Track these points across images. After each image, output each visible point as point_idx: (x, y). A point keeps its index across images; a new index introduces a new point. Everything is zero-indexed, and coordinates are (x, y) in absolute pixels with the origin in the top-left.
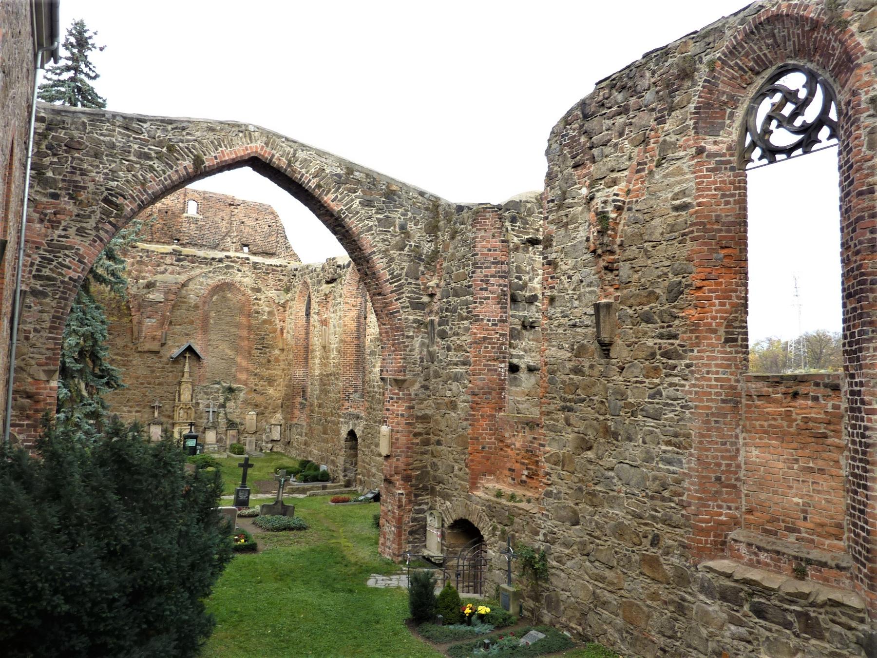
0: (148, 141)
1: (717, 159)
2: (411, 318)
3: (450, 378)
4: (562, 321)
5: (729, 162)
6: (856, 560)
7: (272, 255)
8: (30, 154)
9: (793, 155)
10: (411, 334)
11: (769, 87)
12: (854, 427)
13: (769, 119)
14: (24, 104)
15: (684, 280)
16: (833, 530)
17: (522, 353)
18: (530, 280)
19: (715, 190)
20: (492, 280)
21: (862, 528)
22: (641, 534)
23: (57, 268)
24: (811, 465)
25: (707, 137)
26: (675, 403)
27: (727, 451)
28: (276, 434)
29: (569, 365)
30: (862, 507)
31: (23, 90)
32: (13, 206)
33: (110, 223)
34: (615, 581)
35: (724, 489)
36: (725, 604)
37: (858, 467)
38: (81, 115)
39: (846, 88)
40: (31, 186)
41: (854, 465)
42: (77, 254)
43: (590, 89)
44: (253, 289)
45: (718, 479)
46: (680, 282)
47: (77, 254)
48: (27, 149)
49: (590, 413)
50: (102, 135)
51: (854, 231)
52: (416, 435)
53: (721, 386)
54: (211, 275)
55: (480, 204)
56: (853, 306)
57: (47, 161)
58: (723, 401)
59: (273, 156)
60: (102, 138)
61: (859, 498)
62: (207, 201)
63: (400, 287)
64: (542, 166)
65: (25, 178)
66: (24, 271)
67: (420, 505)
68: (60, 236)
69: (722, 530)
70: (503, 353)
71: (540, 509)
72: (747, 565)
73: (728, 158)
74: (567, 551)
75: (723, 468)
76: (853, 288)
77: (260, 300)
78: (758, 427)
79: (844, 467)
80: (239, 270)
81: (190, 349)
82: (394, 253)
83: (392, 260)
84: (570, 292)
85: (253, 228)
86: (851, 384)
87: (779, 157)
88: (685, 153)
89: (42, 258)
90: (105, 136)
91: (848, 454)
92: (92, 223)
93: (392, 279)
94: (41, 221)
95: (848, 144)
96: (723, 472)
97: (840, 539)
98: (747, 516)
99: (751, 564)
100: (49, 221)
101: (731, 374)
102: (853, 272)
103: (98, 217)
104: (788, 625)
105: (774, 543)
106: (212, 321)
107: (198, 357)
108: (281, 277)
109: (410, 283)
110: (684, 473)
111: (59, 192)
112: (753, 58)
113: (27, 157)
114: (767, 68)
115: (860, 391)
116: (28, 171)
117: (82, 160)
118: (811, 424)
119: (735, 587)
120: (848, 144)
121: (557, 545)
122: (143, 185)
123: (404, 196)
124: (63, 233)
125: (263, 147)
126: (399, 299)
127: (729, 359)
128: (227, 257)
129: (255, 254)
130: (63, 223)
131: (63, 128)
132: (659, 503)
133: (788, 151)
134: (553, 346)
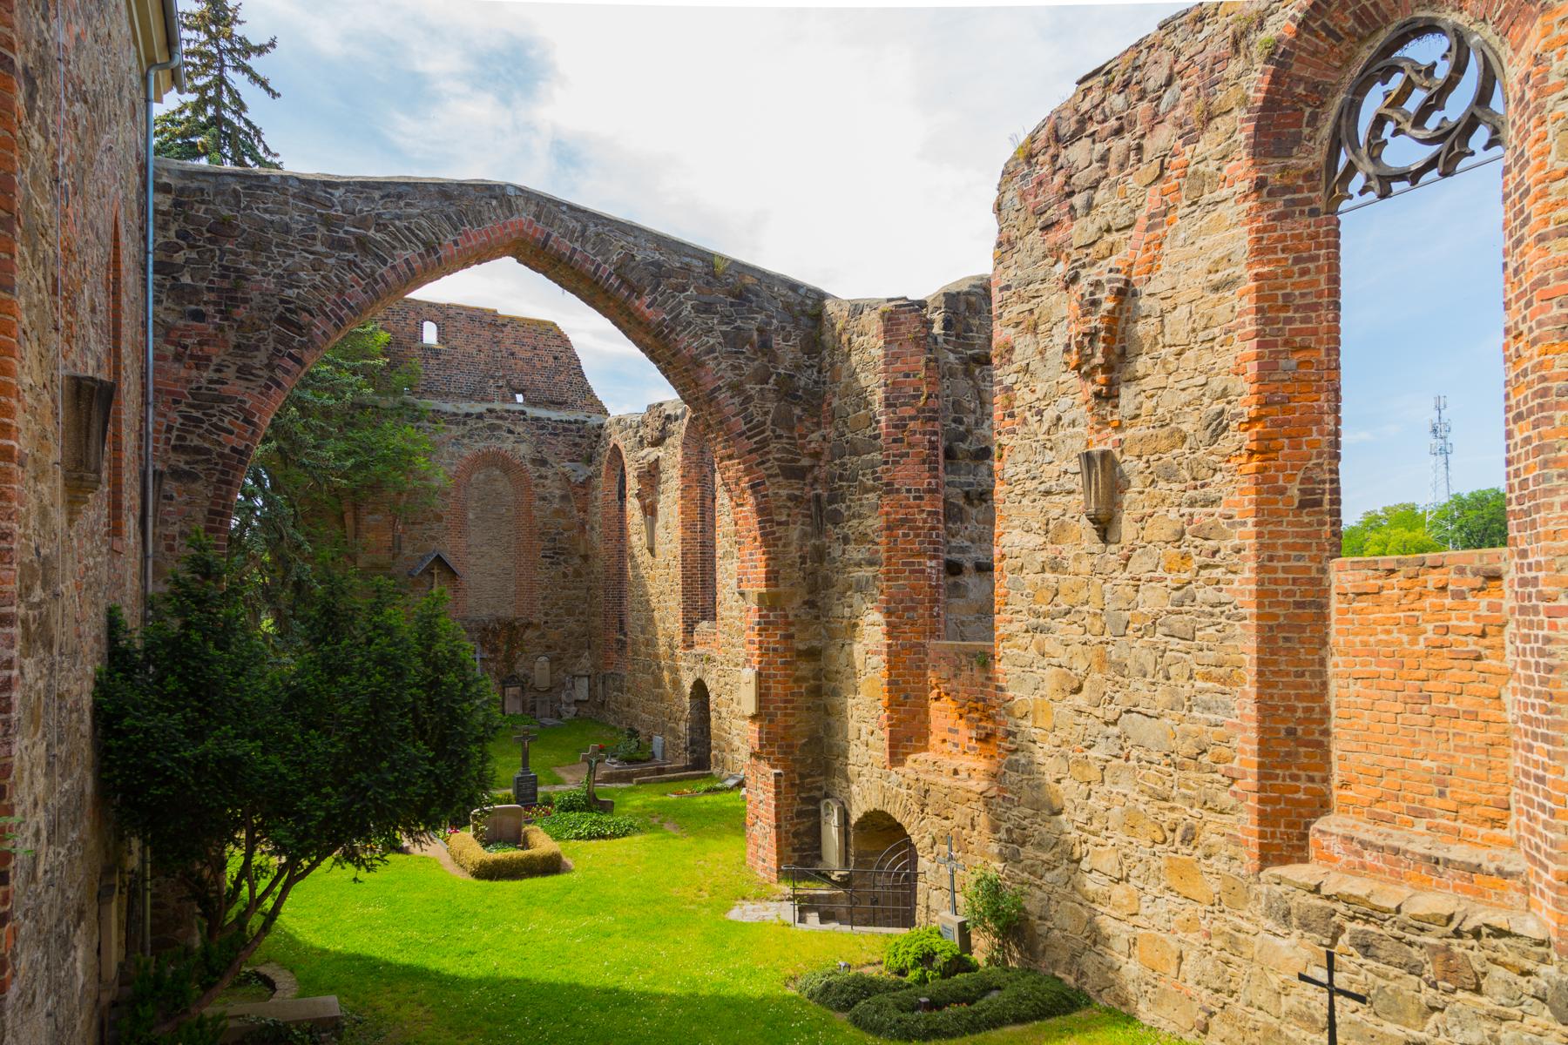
0: (344, 219)
1: (1288, 197)
2: (783, 492)
3: (850, 587)
4: (1029, 485)
5: (1309, 201)
6: (1533, 859)
7: (560, 404)
8: (151, 248)
9: (1422, 181)
10: (784, 519)
11: (1382, 64)
12: (1526, 639)
13: (1380, 121)
14: (133, 164)
15: (1228, 407)
16: (1493, 812)
17: (967, 543)
18: (976, 423)
19: (1283, 251)
20: (911, 425)
21: (1542, 807)
22: (1165, 825)
23: (211, 433)
24: (1452, 705)
25: (1270, 161)
26: (1217, 610)
27: (1306, 686)
28: (582, 692)
29: (1041, 557)
30: (1540, 772)
31: (130, 136)
32: (128, 332)
33: (291, 356)
34: (1125, 902)
35: (1302, 749)
36: (1307, 935)
37: (1533, 705)
38: (230, 179)
39: (1523, 53)
40: (157, 301)
41: (1526, 704)
42: (240, 409)
43: (1068, 89)
44: (533, 461)
45: (1291, 732)
46: (1222, 413)
47: (240, 409)
48: (145, 238)
49: (1075, 634)
50: (266, 211)
51: (1529, 304)
52: (797, 680)
53: (1294, 580)
54: (466, 441)
55: (889, 300)
56: (1526, 434)
57: (179, 258)
58: (1298, 605)
59: (549, 235)
60: (267, 216)
61: (1535, 757)
62: (444, 315)
63: (764, 443)
64: (989, 227)
65: (145, 287)
66: (156, 440)
67: (810, 790)
68: (211, 381)
69: (1300, 815)
70: (934, 543)
71: (1000, 790)
72: (1343, 871)
73: (1306, 194)
74: (1046, 856)
75: (1299, 714)
76: (1526, 402)
77: (546, 478)
78: (1358, 646)
79: (1509, 707)
80: (510, 432)
81: (439, 560)
82: (752, 388)
83: (748, 399)
84: (1041, 437)
85: (529, 361)
86: (1520, 568)
87: (1396, 186)
88: (1232, 190)
89: (184, 417)
90: (271, 213)
91: (1516, 684)
92: (261, 357)
93: (749, 430)
94: (178, 358)
95: (1522, 154)
96: (1299, 721)
97: (1504, 827)
98: (1343, 792)
99: (1351, 870)
100: (191, 356)
101: (1312, 559)
102: (1525, 376)
103: (271, 348)
104: (1415, 969)
105: (1389, 835)
106: (471, 516)
107: (453, 574)
108: (578, 440)
109: (780, 437)
110: (1234, 725)
111: (202, 308)
112: (1354, 13)
113: (147, 252)
114: (1379, 28)
115: (1536, 578)
116: (151, 276)
117: (237, 255)
118: (1451, 637)
119: (1322, 909)
120: (1522, 154)
121: (1028, 847)
122: (341, 293)
123: (765, 293)
124: (216, 376)
125: (531, 223)
126: (763, 463)
127: (1307, 535)
128: (490, 411)
129: (534, 404)
130: (215, 360)
131: (203, 202)
132: (1193, 774)
133: (1414, 177)
134: (1014, 528)
